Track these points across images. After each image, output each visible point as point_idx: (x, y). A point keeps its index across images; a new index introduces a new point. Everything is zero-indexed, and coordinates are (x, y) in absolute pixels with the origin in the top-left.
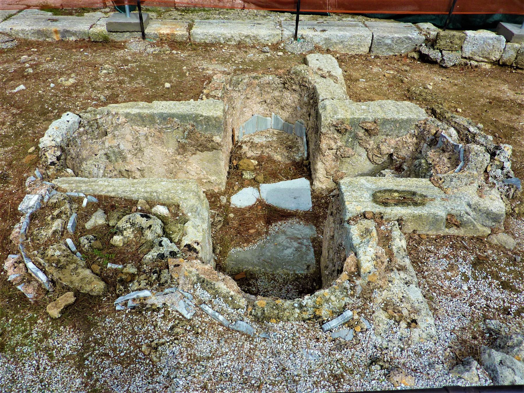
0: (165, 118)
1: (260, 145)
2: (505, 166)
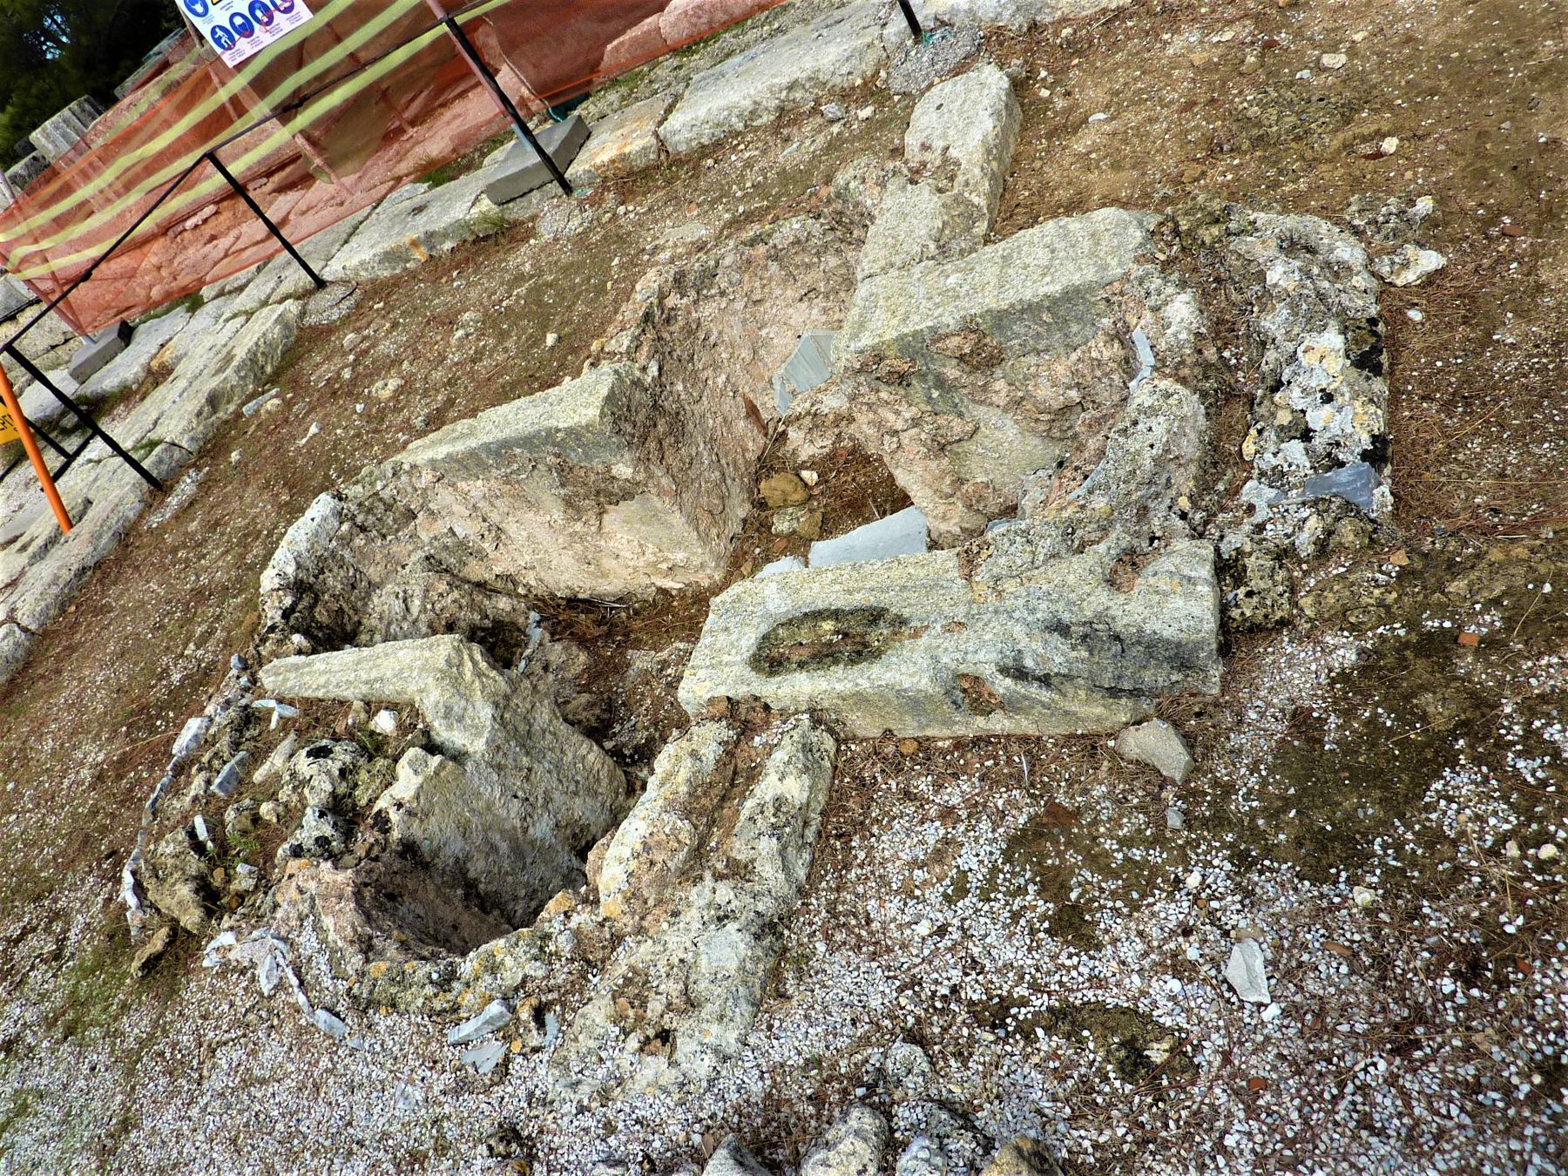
0: (501, 451)
1: (831, 417)
2: (1311, 425)
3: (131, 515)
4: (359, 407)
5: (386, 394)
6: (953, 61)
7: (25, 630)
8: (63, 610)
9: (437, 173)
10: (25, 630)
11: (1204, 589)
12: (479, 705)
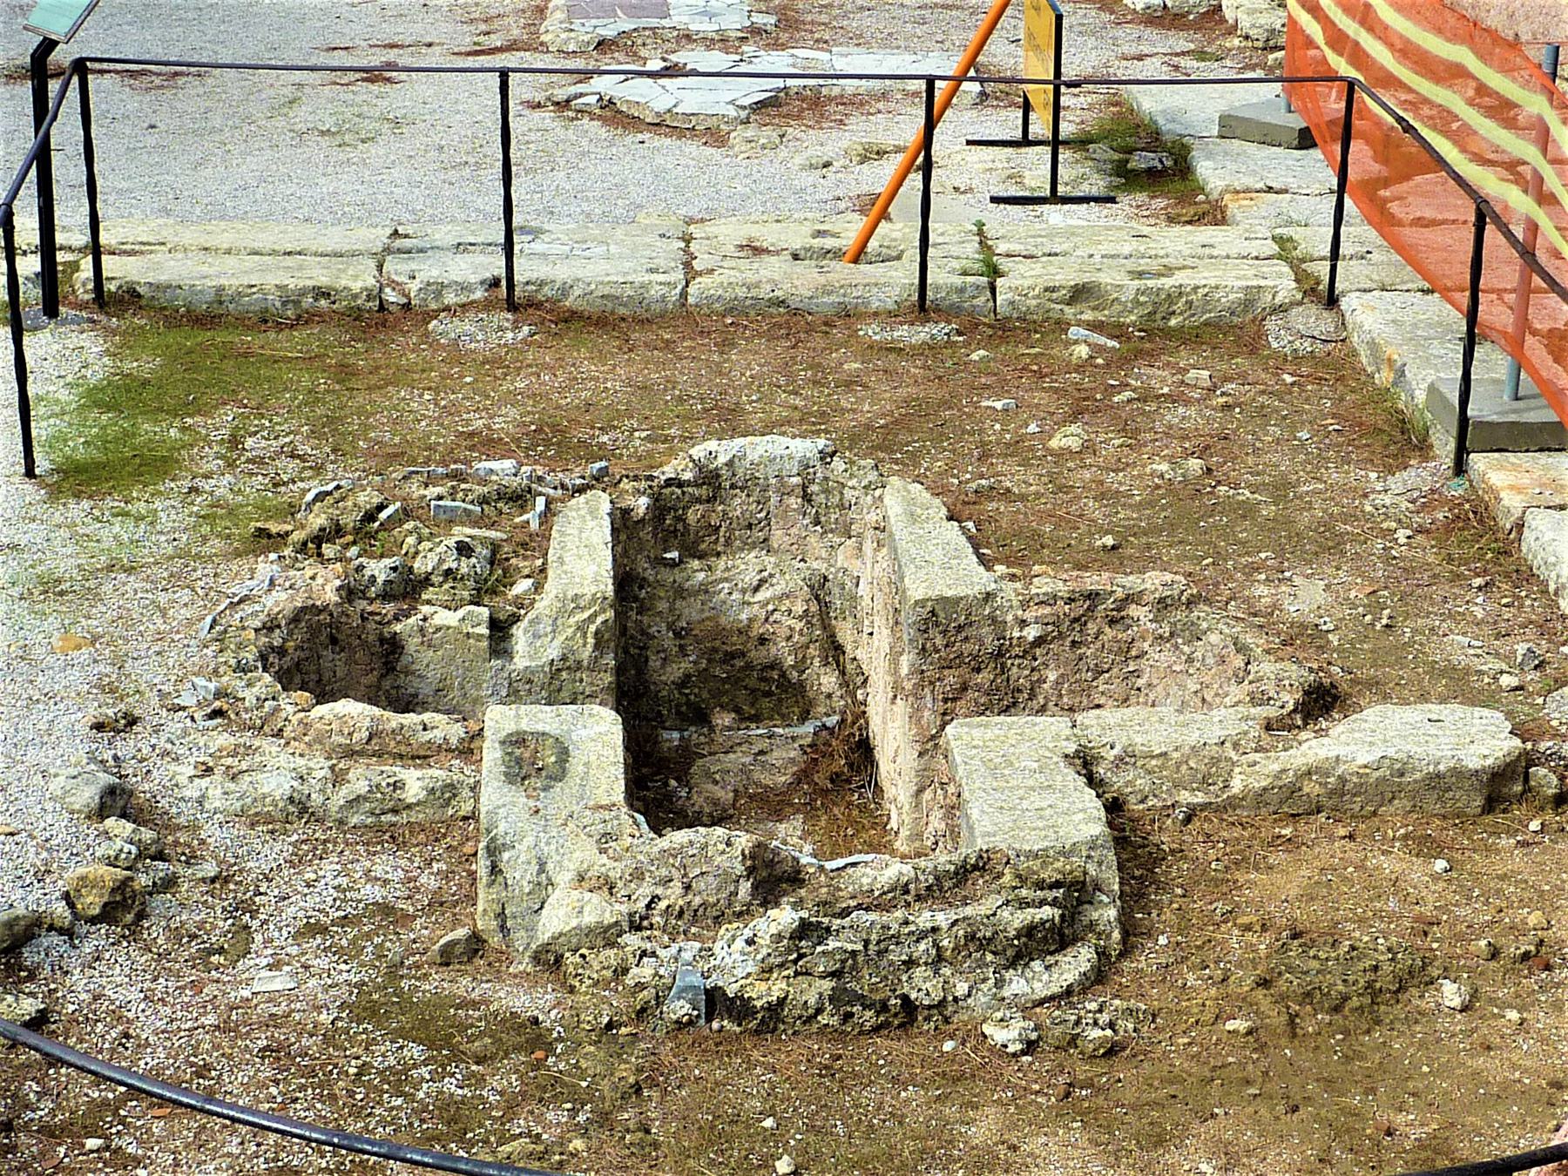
3: (875, 305)
7: (684, 294)
10: (684, 294)
11: (574, 923)
12: (556, 643)
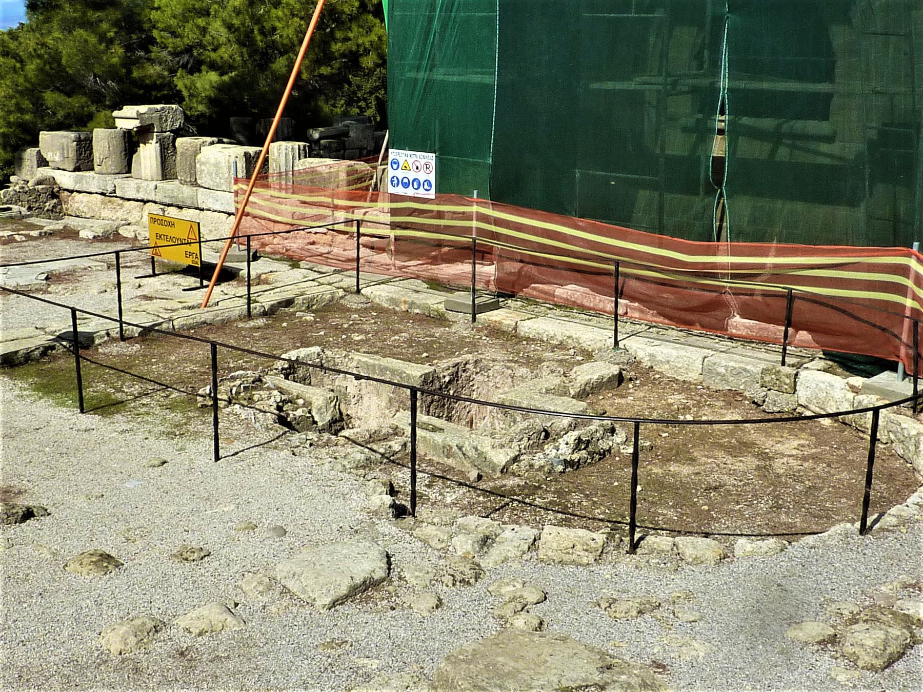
4: (344, 337)
5: (357, 338)
6: (617, 361)
8: (189, 329)
9: (436, 284)
